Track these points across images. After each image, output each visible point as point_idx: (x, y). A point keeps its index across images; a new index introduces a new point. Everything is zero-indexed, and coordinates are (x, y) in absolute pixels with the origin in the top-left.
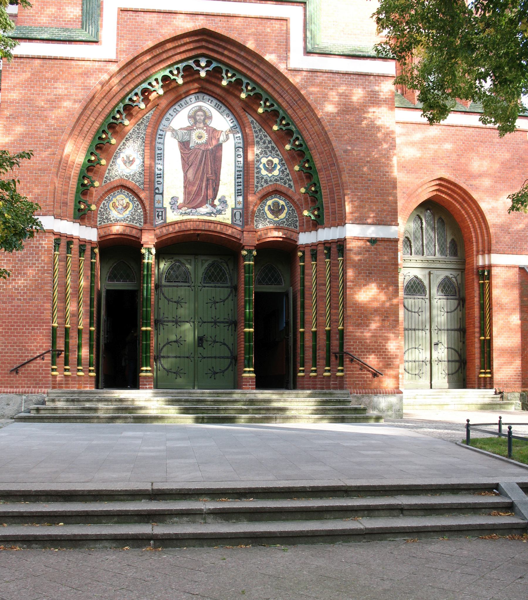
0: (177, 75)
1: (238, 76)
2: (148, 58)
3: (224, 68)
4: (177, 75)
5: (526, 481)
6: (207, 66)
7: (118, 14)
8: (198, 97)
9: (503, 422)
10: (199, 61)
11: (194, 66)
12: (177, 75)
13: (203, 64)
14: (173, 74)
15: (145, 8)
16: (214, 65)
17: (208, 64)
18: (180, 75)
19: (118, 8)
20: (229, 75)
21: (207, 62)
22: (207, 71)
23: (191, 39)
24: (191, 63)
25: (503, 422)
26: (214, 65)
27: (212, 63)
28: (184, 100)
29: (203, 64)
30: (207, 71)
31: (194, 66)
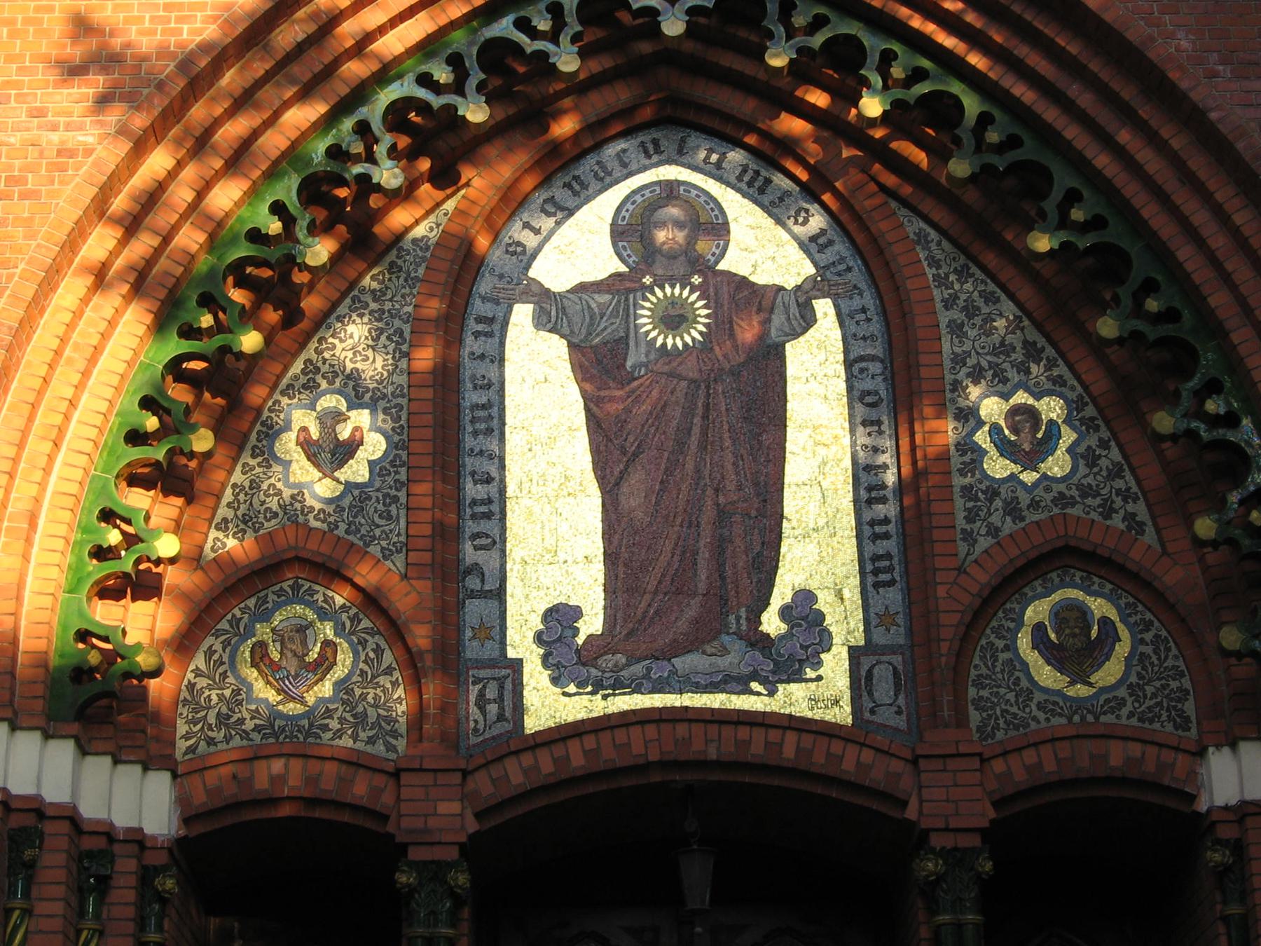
4: (458, 87)
8: (656, 143)
12: (554, 37)
14: (534, 34)
18: (565, 39)
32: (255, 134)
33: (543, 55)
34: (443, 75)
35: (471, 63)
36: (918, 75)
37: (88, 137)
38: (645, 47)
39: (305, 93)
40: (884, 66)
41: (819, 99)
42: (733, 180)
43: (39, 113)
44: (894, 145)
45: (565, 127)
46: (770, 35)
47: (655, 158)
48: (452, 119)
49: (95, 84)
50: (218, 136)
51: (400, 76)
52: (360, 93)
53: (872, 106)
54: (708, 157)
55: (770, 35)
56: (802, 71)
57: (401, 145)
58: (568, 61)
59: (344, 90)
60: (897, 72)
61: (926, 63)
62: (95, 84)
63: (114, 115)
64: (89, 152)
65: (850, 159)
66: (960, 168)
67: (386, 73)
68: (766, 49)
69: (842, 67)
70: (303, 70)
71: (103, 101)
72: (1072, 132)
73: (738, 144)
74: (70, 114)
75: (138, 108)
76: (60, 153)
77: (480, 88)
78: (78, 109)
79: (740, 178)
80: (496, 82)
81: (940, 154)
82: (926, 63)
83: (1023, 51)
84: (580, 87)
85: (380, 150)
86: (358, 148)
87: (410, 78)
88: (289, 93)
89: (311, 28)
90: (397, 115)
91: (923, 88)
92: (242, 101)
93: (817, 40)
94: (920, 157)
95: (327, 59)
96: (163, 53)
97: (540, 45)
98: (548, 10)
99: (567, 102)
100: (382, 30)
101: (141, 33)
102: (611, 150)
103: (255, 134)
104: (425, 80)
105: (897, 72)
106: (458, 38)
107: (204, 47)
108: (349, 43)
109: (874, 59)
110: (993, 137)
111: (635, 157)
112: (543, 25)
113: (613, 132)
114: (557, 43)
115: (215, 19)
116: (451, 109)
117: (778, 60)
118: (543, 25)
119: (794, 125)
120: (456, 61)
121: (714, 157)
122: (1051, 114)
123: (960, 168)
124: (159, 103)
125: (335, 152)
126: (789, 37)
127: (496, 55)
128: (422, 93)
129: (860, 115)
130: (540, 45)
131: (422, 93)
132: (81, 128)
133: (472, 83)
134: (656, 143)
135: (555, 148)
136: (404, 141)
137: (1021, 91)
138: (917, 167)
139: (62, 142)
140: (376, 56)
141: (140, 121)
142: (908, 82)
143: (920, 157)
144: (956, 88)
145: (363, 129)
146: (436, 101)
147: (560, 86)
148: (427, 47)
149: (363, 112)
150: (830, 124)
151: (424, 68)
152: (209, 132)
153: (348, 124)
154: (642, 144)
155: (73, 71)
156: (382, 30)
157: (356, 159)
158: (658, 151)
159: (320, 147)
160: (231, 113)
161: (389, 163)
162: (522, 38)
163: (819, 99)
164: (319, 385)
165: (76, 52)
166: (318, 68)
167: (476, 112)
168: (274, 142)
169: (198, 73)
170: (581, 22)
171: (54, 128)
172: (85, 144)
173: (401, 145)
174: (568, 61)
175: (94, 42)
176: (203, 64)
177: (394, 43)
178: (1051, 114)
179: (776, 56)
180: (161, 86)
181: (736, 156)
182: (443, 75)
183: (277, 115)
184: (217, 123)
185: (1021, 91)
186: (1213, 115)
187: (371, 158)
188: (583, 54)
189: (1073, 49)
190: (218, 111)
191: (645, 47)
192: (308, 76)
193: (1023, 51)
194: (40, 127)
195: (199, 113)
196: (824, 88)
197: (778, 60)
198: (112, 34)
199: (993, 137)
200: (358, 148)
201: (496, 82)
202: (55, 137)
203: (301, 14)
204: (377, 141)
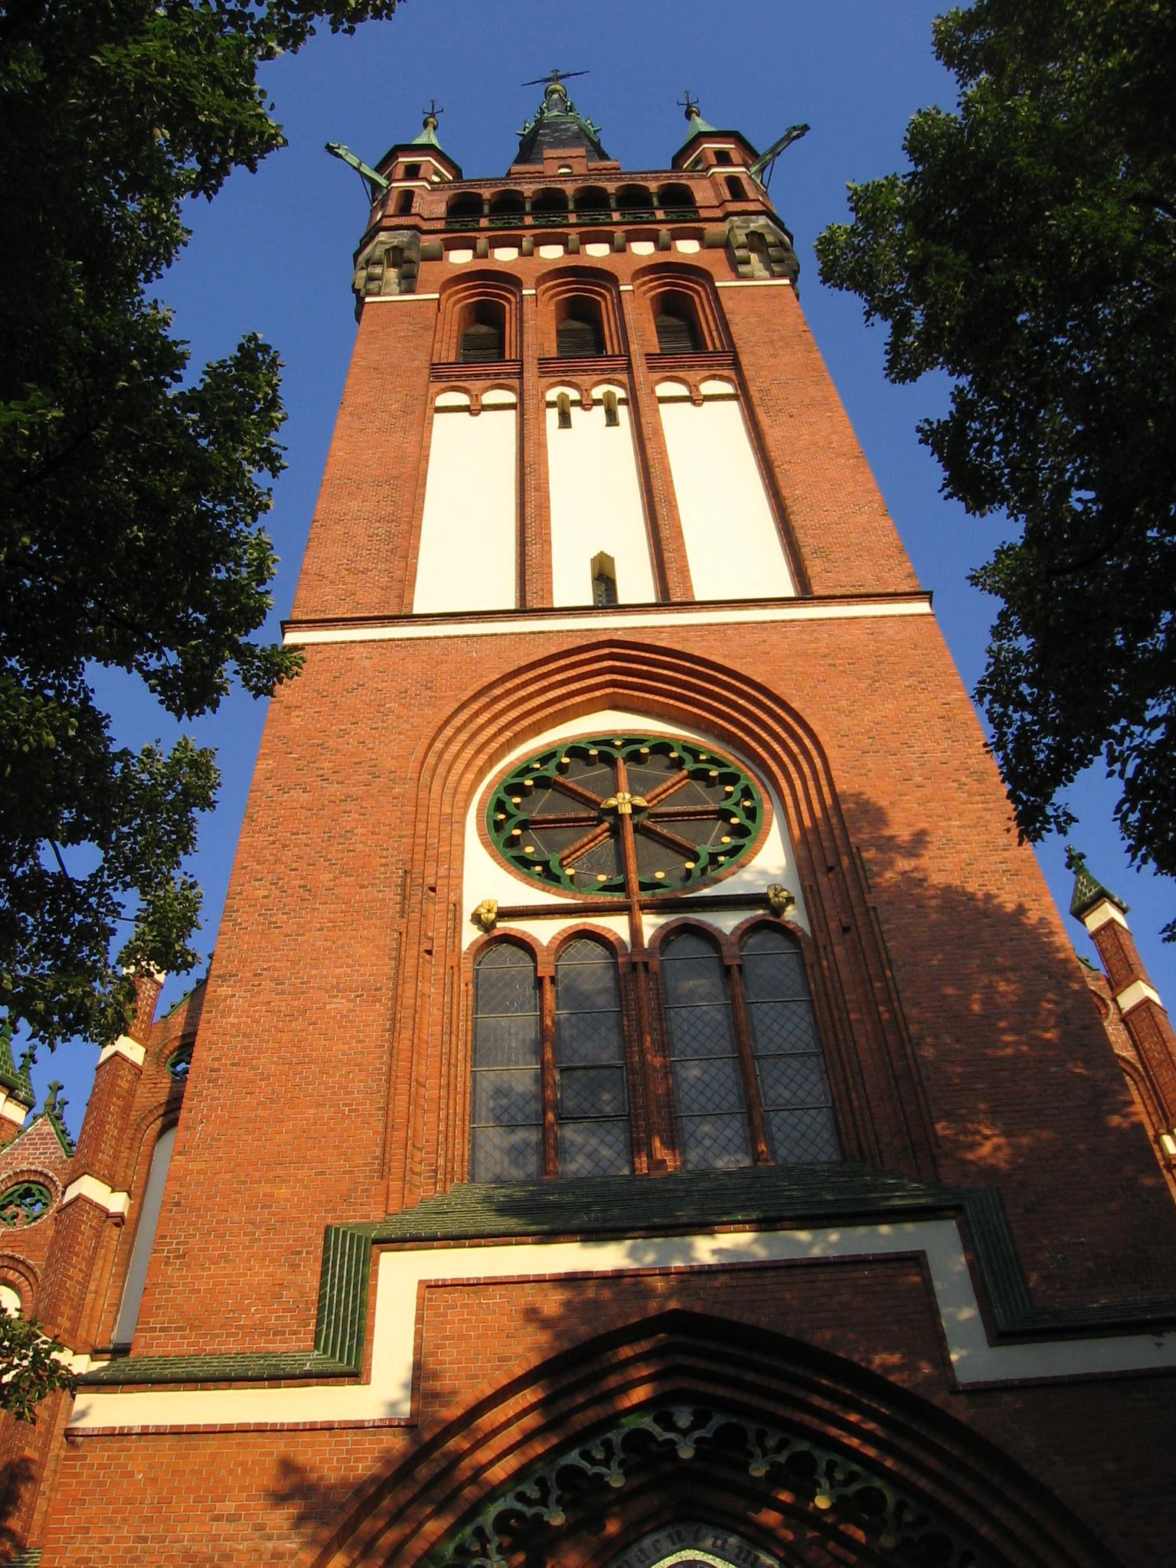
0: (606, 1463)
1: (803, 1446)
2: (645, 1373)
3: (752, 1428)
4: (543, 1501)
5: (1173, 1364)
6: (694, 1427)
7: (420, 1298)
8: (679, 1534)
9: (511, 414)
10: (670, 1415)
11: (656, 1430)
12: (606, 1463)
13: (684, 1419)
14: (593, 1462)
15: (531, 1273)
16: (718, 1420)
17: (698, 1422)
18: (614, 1464)
19: (421, 1282)
20: (771, 1443)
21: (693, 1414)
22: (699, 1441)
23: (644, 1346)
24: (573, 1457)
25: (511, 414)
26: (718, 1420)
27: (711, 1418)
28: (635, 1548)
29: (684, 1419)
30: (699, 1441)
31: (656, 1430)
32: (406, 1539)
33: (600, 1476)
34: (533, 1493)
35: (552, 1483)
36: (853, 1477)
37: (291, 1545)
38: (668, 1467)
39: (437, 1513)
40: (829, 1475)
41: (785, 1497)
42: (733, 1557)
43: (260, 1527)
44: (842, 1527)
45: (612, 1527)
46: (751, 1455)
47: (678, 1546)
48: (539, 1522)
49: (291, 1510)
50: (381, 1541)
51: (504, 1495)
52: (476, 1509)
53: (822, 1502)
54: (715, 1543)
55: (751, 1455)
56: (776, 1478)
57: (505, 1545)
58: (617, 1481)
59: (466, 1506)
60: (839, 1476)
61: (855, 1467)
62: (291, 1510)
63: (308, 1529)
64: (293, 1554)
65: (812, 1539)
66: (887, 1541)
67: (494, 1493)
68: (748, 1465)
69: (801, 1476)
70: (439, 1494)
71: (300, 1521)
72: (961, 1510)
73: (733, 1531)
74: (281, 1528)
75: (327, 1524)
76: (273, 1556)
77: (559, 1501)
78: (286, 1525)
79: (738, 1557)
80: (568, 1496)
81: (872, 1531)
82: (855, 1467)
83: (921, 1455)
84: (624, 1497)
85: (491, 1547)
86: (476, 1547)
87: (511, 1496)
88: (428, 1510)
89: (444, 1463)
90: (502, 1522)
91: (855, 1487)
92: (397, 1517)
93: (782, 1458)
94: (860, 1535)
95: (455, 1484)
96: (344, 1483)
97: (597, 1469)
98: (602, 1444)
99: (616, 1509)
100: (492, 1463)
101: (330, 1469)
102: (647, 1542)
103: (406, 1539)
104: (521, 1497)
105: (839, 1476)
106: (541, 1470)
107: (373, 1479)
108: (469, 1473)
109: (822, 1466)
110: (908, 1517)
111: (667, 1545)
112: (599, 1455)
113: (647, 1528)
114: (609, 1468)
115: (379, 1459)
116: (539, 1517)
117: (758, 1470)
118: (599, 1455)
119: (770, 1517)
120: (541, 1483)
121: (719, 1543)
122: (945, 1498)
123: (887, 1541)
124: (342, 1519)
125: (462, 1551)
126: (765, 1455)
127: (570, 1477)
128: (519, 1506)
129: (816, 1507)
130: (597, 1469)
131: (519, 1506)
132: (288, 1538)
133: (553, 1498)
134: (679, 1534)
135: (609, 1542)
136: (507, 1541)
137: (923, 1483)
138: (857, 1542)
139: (275, 1548)
140: (487, 1482)
141: (326, 1534)
142: (847, 1483)
143: (860, 1535)
144: (878, 1483)
145: (479, 1533)
146: (530, 1512)
147: (611, 1497)
148: (518, 1476)
149: (480, 1520)
150: (799, 1515)
151: (520, 1489)
152: (375, 1538)
153: (468, 1530)
154: (670, 1535)
155: (279, 1499)
156: (492, 1463)
157: (475, 1555)
158: (681, 1540)
159: (449, 1550)
160: (389, 1526)
161: (498, 1557)
162: (585, 1464)
163: (785, 1497)
164: (1147, 1002)
165: (285, 1485)
166: (448, 1491)
167: (557, 1519)
168: (417, 1546)
169: (367, 1496)
170: (624, 1452)
171: (270, 1538)
172: (291, 1549)
173: (505, 1545)
174: (617, 1481)
175: (294, 1479)
176: (372, 1490)
177: (498, 1473)
178: (945, 1498)
179: (757, 1469)
180: (342, 1506)
181: (733, 1540)
182: (533, 1493)
183: (421, 1524)
184: (381, 1532)
185: (923, 1483)
186: (1057, 1492)
187: (485, 1554)
188: (627, 1474)
189: (956, 1452)
190: (381, 1524)
191: (668, 1467)
192: (442, 1497)
193: (921, 1455)
194: (260, 1538)
195: (367, 1526)
196: (790, 1489)
197: (758, 1470)
198: (311, 1471)
199: (908, 1517)
200: (476, 1547)
201: (568, 1496)
202: (270, 1545)
203: (436, 1455)
204: (489, 1541)
